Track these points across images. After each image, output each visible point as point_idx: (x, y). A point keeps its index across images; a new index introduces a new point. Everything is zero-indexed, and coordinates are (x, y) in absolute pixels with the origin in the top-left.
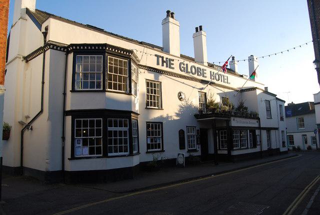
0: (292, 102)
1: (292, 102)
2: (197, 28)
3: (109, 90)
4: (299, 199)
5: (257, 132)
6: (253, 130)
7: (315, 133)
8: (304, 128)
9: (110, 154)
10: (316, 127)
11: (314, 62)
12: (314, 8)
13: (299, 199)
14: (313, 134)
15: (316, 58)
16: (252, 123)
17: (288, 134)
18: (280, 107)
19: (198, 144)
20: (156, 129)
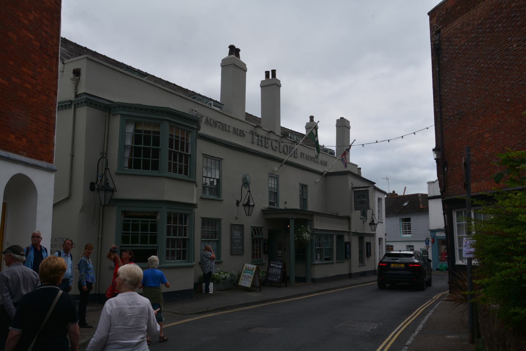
0: (394, 192)
1: (394, 192)
2: (267, 73)
3: (168, 174)
4: (416, 313)
5: (346, 239)
6: (340, 237)
7: (427, 243)
8: (410, 235)
9: (320, 271)
10: (429, 235)
11: (434, 150)
12: (439, 75)
13: (416, 313)
14: (423, 246)
15: (436, 145)
16: (340, 227)
17: (387, 244)
18: (378, 202)
19: (265, 252)
20: (175, 222)
